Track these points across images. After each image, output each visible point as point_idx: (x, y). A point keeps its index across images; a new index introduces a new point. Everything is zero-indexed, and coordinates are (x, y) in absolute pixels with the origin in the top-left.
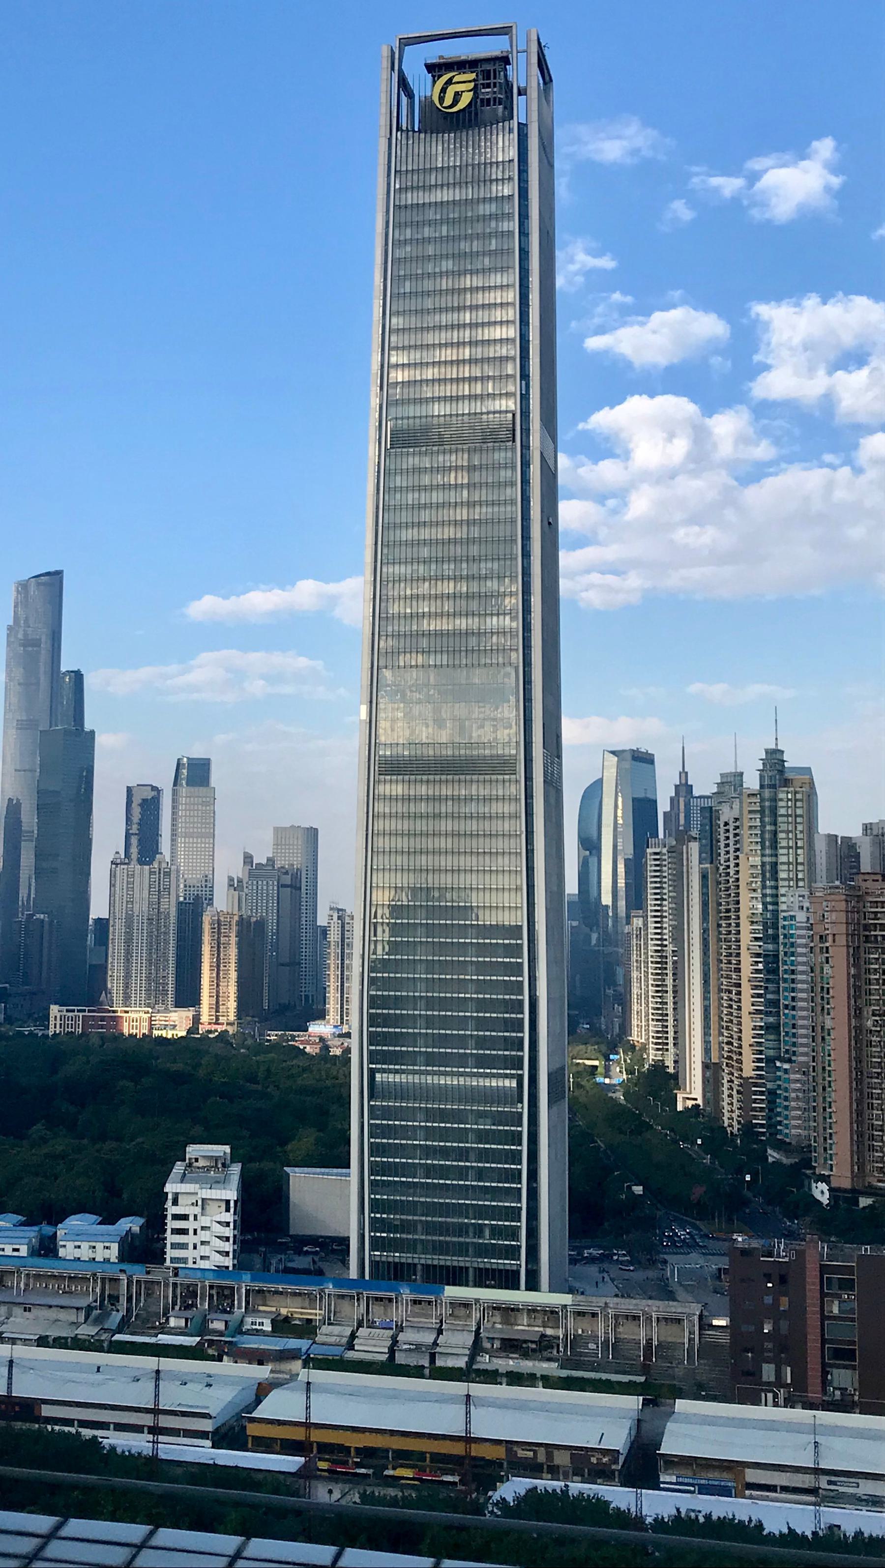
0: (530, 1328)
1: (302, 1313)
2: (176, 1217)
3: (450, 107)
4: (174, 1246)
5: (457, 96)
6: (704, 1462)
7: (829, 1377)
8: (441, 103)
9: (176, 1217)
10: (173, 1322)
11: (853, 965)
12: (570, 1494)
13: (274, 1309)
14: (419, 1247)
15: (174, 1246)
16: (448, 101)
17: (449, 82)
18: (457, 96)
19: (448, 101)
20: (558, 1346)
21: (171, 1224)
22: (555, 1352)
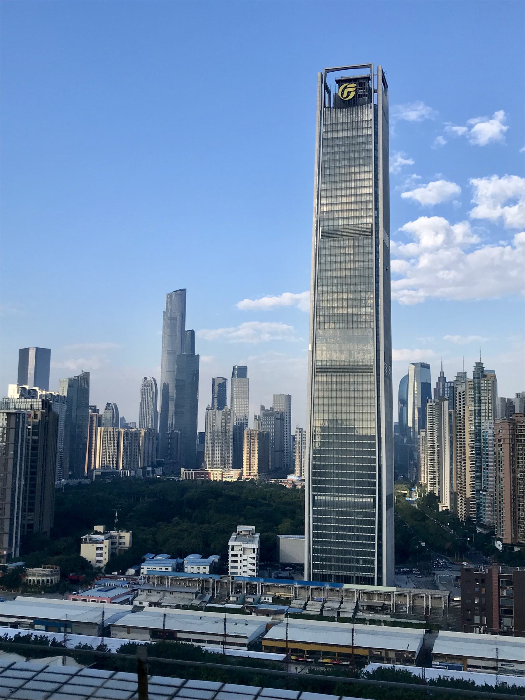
2: (233, 555)
3: (346, 98)
5: (349, 93)
8: (342, 95)
9: (233, 555)
11: (512, 452)
14: (333, 568)
15: (232, 567)
16: (345, 95)
17: (345, 87)
18: (349, 93)
19: (345, 95)
21: (231, 558)
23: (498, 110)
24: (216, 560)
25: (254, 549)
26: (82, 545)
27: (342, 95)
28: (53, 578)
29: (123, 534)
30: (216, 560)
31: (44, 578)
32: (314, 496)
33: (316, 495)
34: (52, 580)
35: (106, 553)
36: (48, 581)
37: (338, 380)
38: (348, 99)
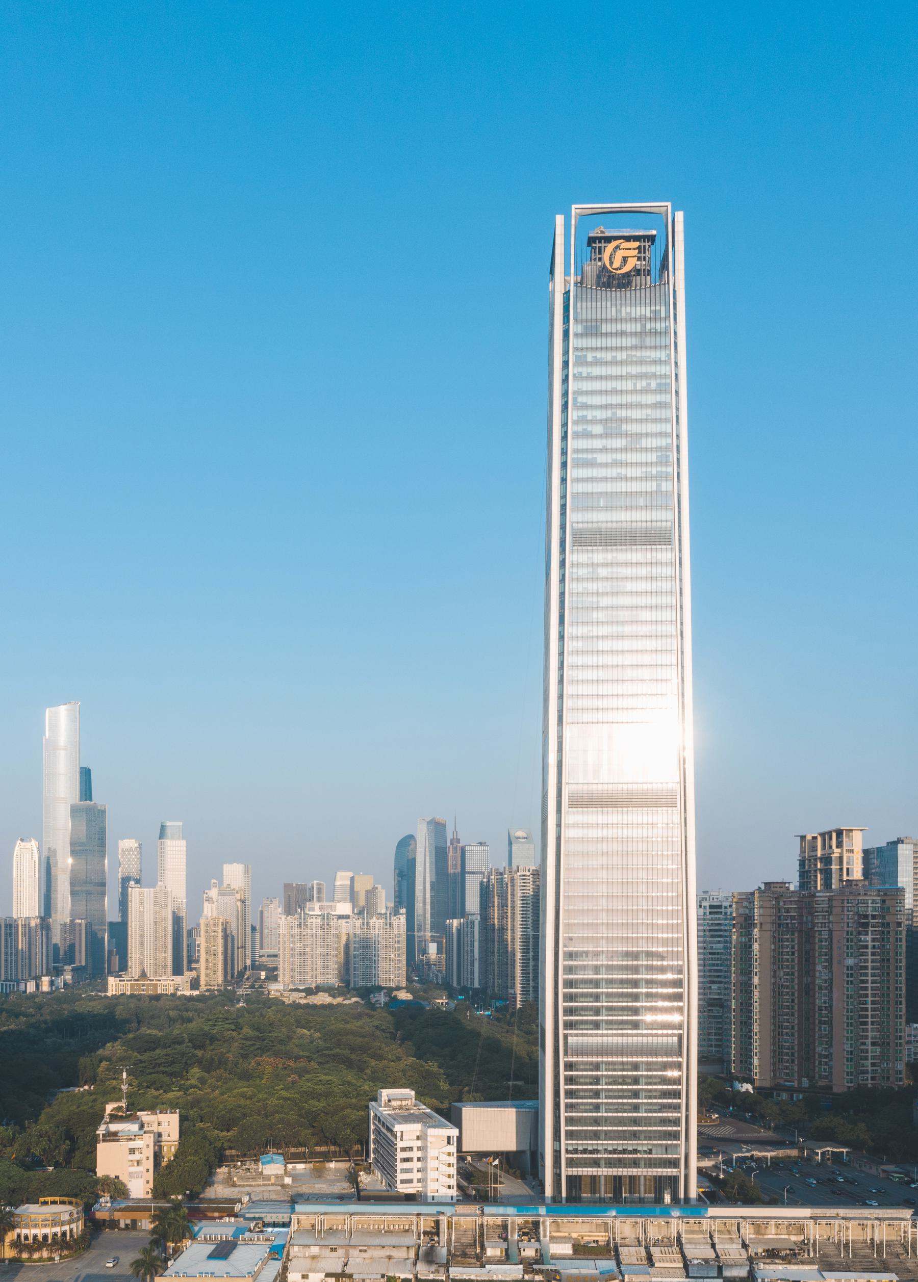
0: (777, 1237)
1: (590, 1236)
2: (403, 1149)
4: (404, 1171)
5: (625, 259)
6: (200, 1005)
7: (773, 947)
9: (403, 1149)
10: (490, 1252)
12: (152, 1226)
13: (566, 1234)
14: (642, 1164)
15: (404, 1171)
16: (617, 264)
17: (617, 247)
18: (625, 259)
19: (617, 264)
20: (809, 1250)
21: (400, 1155)
22: (806, 1256)
23: (55, 702)
24: (111, 980)
25: (449, 1137)
26: (101, 1148)
27: (611, 263)
28: (74, 1226)
29: (163, 1118)
30: (111, 980)
31: (57, 1230)
32: (566, 1037)
33: (572, 1035)
34: (71, 1231)
35: (148, 1158)
36: (64, 1234)
37: (615, 830)
38: (623, 271)
